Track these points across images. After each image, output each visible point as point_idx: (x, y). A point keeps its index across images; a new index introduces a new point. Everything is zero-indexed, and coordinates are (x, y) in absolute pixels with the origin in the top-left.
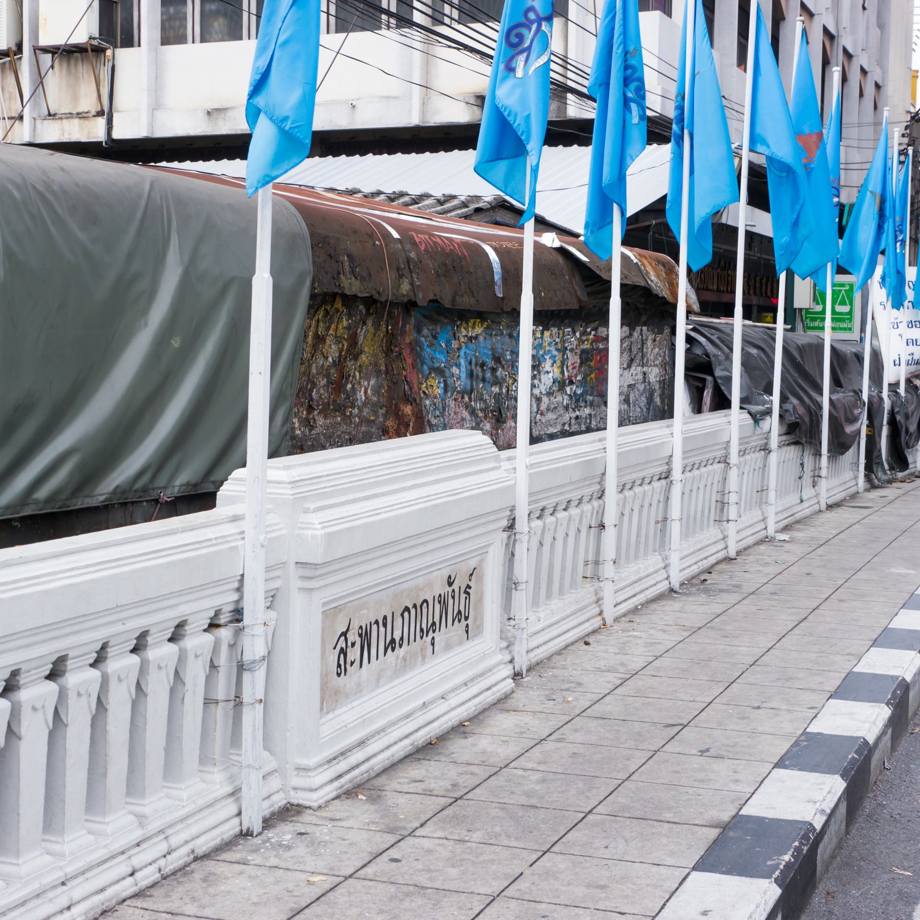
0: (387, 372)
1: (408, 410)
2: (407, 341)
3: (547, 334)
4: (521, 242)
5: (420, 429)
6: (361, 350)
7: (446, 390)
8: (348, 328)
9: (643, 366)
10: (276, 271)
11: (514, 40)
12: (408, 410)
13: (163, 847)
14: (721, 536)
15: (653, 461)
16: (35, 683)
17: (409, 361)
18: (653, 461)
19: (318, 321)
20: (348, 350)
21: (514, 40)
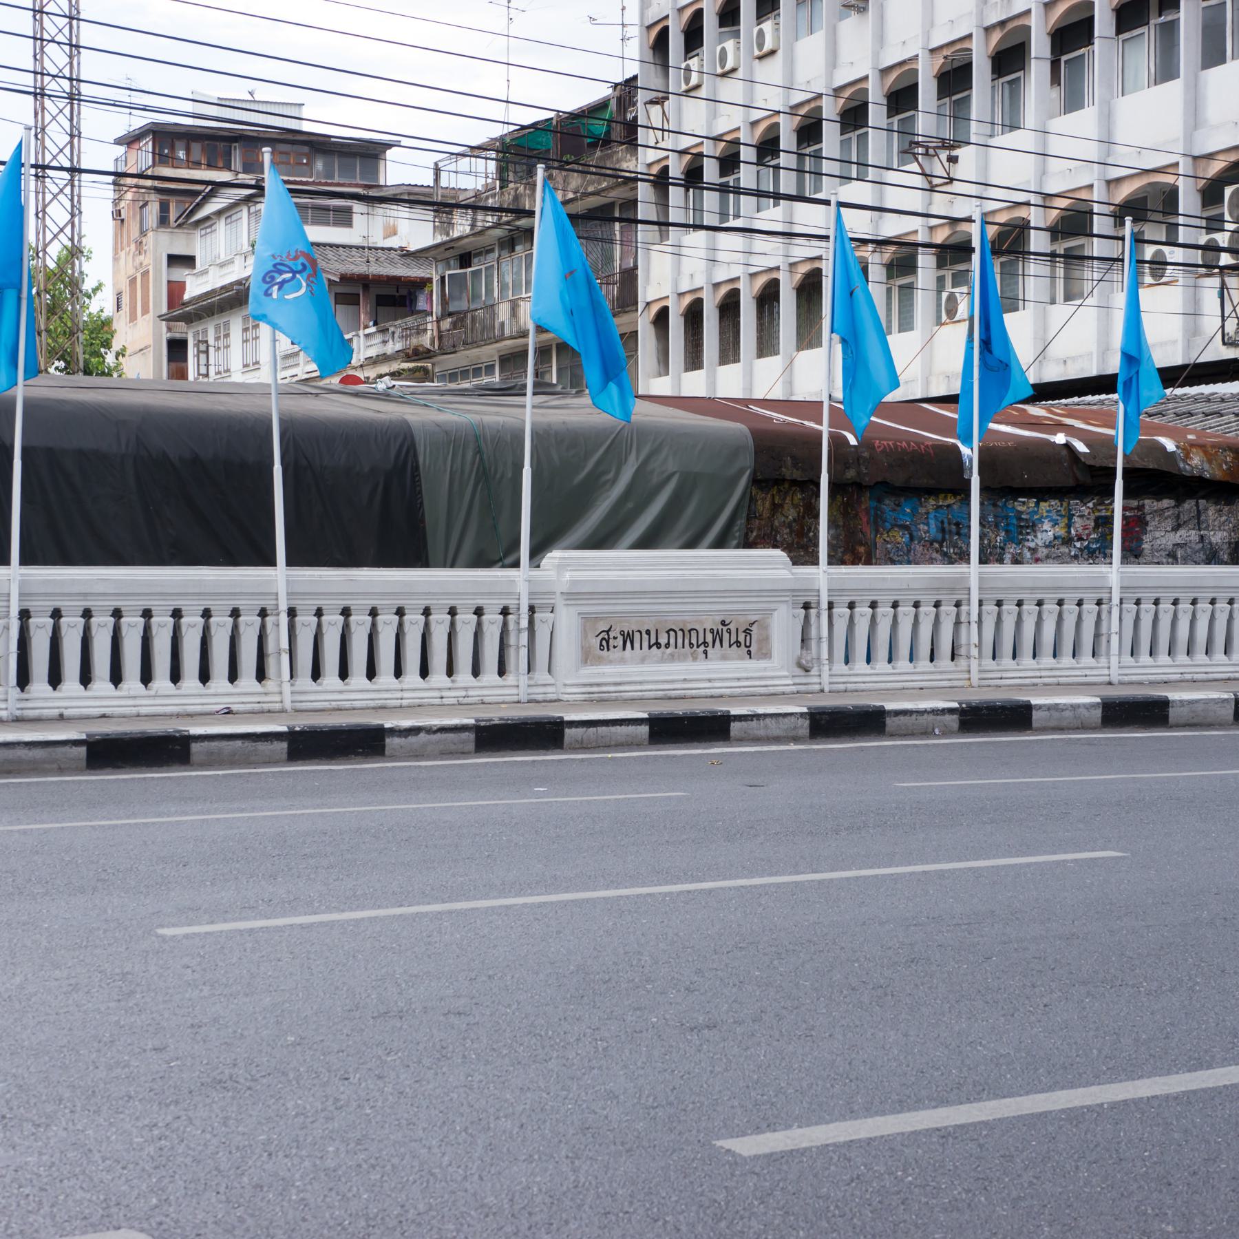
0: (844, 526)
1: (862, 549)
2: (863, 507)
3: (1043, 504)
4: (830, 426)
5: (868, 562)
6: (1034, 525)
7: (912, 538)
8: (803, 499)
9: (1200, 529)
10: (829, 471)
11: (268, 279)
12: (862, 549)
13: (464, 693)
14: (1106, 665)
15: (959, 589)
16: (159, 590)
17: (865, 520)
18: (959, 589)
19: (773, 495)
20: (804, 513)
21: (268, 279)
